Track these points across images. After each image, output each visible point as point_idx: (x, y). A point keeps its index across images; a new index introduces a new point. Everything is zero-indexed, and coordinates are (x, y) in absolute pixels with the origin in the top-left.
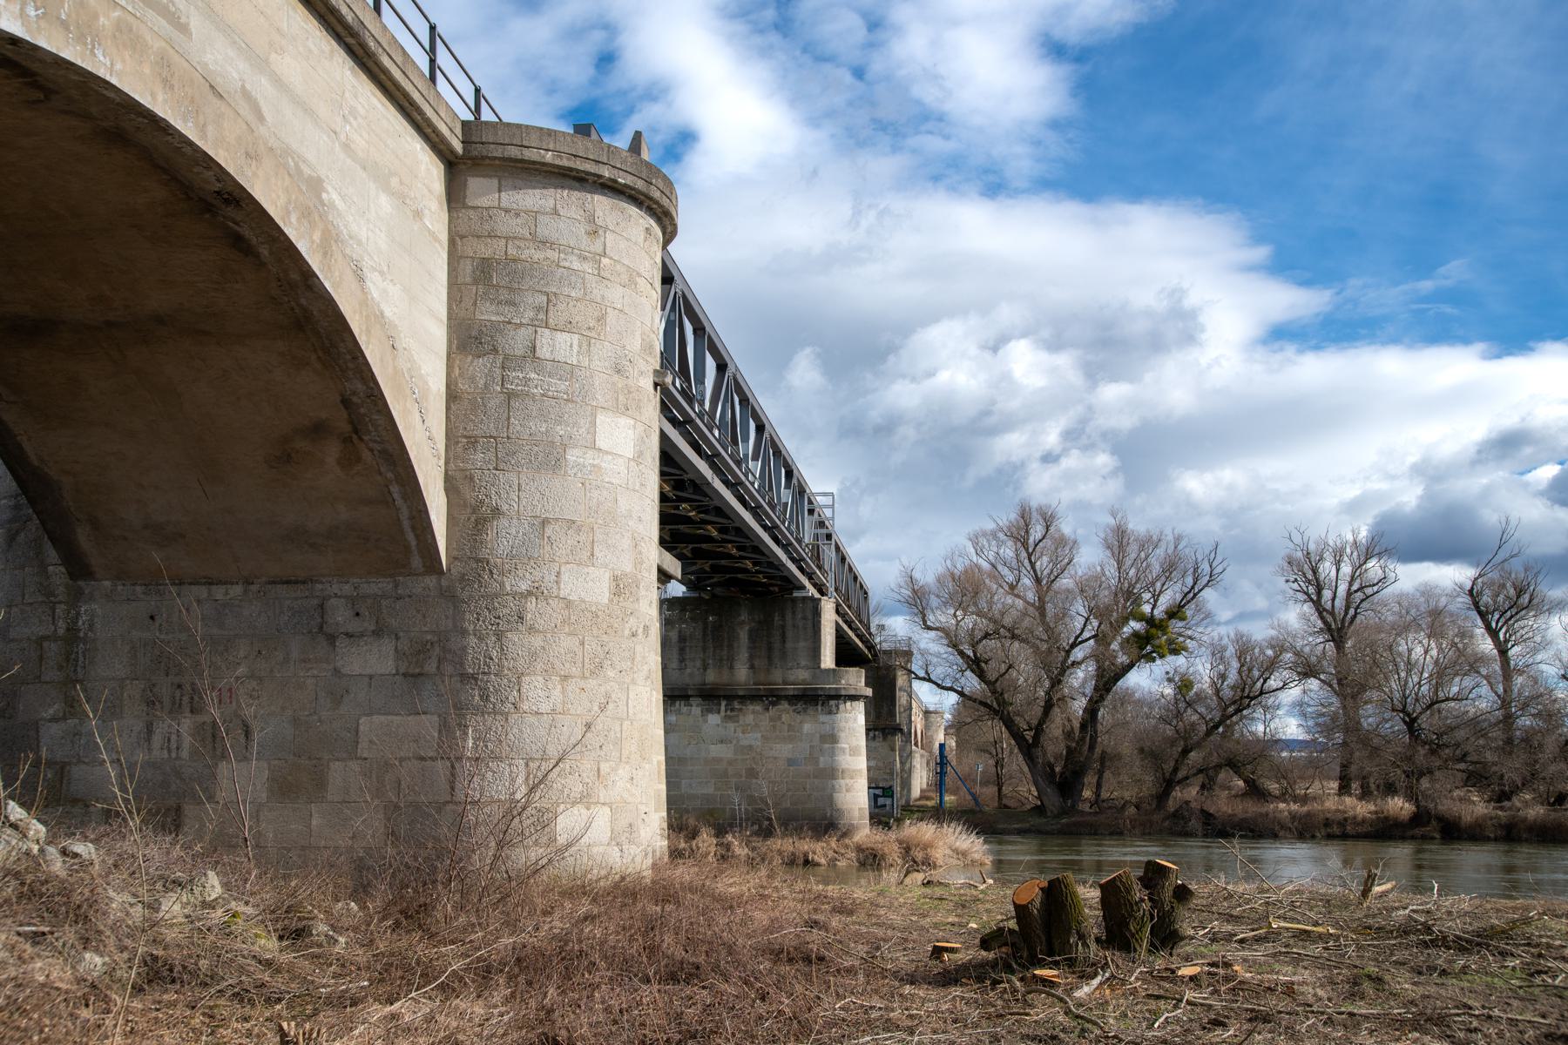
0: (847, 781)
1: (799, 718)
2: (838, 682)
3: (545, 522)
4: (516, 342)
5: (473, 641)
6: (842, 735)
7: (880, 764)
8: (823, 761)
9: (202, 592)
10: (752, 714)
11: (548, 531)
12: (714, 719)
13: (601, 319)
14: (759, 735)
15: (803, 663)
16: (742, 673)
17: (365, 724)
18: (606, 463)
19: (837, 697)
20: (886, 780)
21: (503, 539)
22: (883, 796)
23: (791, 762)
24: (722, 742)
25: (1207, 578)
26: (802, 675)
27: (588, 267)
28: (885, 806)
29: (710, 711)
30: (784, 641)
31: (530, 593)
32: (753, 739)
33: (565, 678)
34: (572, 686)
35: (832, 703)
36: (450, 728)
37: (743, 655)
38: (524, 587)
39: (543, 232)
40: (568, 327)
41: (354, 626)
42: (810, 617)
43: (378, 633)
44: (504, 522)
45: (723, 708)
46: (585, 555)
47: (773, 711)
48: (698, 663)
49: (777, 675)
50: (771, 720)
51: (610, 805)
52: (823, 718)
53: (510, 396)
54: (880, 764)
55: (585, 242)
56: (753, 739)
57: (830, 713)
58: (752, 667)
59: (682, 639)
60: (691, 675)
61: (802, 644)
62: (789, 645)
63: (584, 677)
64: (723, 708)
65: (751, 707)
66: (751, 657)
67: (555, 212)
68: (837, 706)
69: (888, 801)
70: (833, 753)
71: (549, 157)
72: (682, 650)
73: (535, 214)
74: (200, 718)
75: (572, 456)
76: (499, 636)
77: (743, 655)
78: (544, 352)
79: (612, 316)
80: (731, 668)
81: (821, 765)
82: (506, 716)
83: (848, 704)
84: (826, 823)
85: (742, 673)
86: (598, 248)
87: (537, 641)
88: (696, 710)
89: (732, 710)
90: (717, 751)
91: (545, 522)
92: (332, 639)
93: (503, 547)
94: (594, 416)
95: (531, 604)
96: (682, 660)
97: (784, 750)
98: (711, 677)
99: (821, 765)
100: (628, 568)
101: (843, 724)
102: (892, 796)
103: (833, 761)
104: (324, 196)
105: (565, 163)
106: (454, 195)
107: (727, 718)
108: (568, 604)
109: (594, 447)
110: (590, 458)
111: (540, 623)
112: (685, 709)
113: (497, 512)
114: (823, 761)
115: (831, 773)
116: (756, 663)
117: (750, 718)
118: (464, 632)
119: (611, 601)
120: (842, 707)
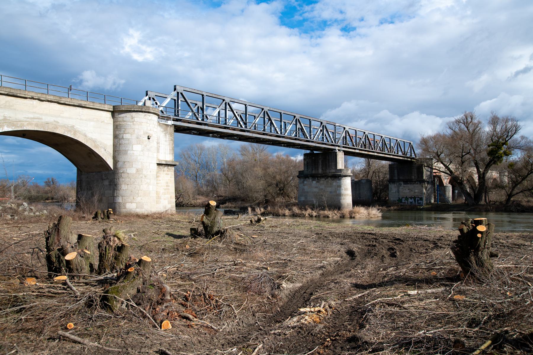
0: (344, 197)
1: (333, 181)
2: (341, 172)
3: (125, 162)
4: (121, 136)
5: (116, 180)
6: (342, 185)
7: (419, 191)
8: (338, 192)
9: (91, 174)
10: (322, 181)
11: (125, 163)
12: (314, 182)
13: (134, 131)
14: (324, 186)
15: (333, 168)
16: (320, 171)
17: (106, 192)
18: (135, 152)
19: (341, 176)
20: (420, 195)
21: (119, 165)
22: (420, 200)
23: (331, 192)
24: (316, 188)
25: (514, 132)
26: (333, 171)
27: (131, 124)
28: (420, 203)
29: (313, 180)
30: (329, 163)
31: (122, 173)
32: (322, 187)
33: (128, 184)
34: (129, 186)
35: (340, 177)
36: (114, 192)
37: (320, 166)
38: (122, 172)
39: (124, 120)
40: (128, 133)
41: (105, 178)
42: (335, 156)
43: (107, 179)
44: (119, 162)
45: (316, 179)
46: (131, 166)
47: (327, 180)
48: (311, 169)
49: (328, 171)
50: (327, 182)
51: (136, 203)
52: (338, 181)
53: (120, 144)
54: (419, 191)
55: (131, 120)
56: (322, 187)
57: (339, 180)
58: (322, 169)
59: (307, 163)
60: (309, 172)
61: (333, 163)
62: (330, 164)
63: (131, 184)
64: (316, 179)
65: (322, 179)
66: (322, 167)
67: (126, 116)
68: (341, 178)
69: (421, 202)
70: (340, 190)
71: (123, 109)
72: (307, 166)
73: (123, 117)
74: (92, 191)
75: (129, 152)
76: (119, 179)
77: (320, 166)
78: (124, 137)
79: (136, 130)
80: (318, 170)
81: (337, 193)
82: (119, 190)
83: (344, 178)
84: (337, 206)
85: (320, 171)
86: (133, 120)
87: (123, 179)
88: (311, 180)
89: (318, 180)
90: (316, 190)
91: (125, 162)
92: (103, 180)
93: (119, 167)
94: (133, 145)
95: (123, 174)
96: (307, 168)
97: (329, 189)
98: (314, 172)
99: (337, 193)
100: (140, 167)
101: (342, 183)
102: (422, 200)
103: (340, 192)
104: (75, 127)
105: (126, 110)
106: (113, 116)
107: (317, 182)
108: (128, 174)
109: (133, 150)
110: (132, 152)
111: (124, 177)
112: (308, 180)
113: (118, 161)
114: (338, 192)
115: (339, 195)
116: (323, 168)
117: (322, 182)
118: (115, 179)
119: (136, 173)
120: (342, 179)
